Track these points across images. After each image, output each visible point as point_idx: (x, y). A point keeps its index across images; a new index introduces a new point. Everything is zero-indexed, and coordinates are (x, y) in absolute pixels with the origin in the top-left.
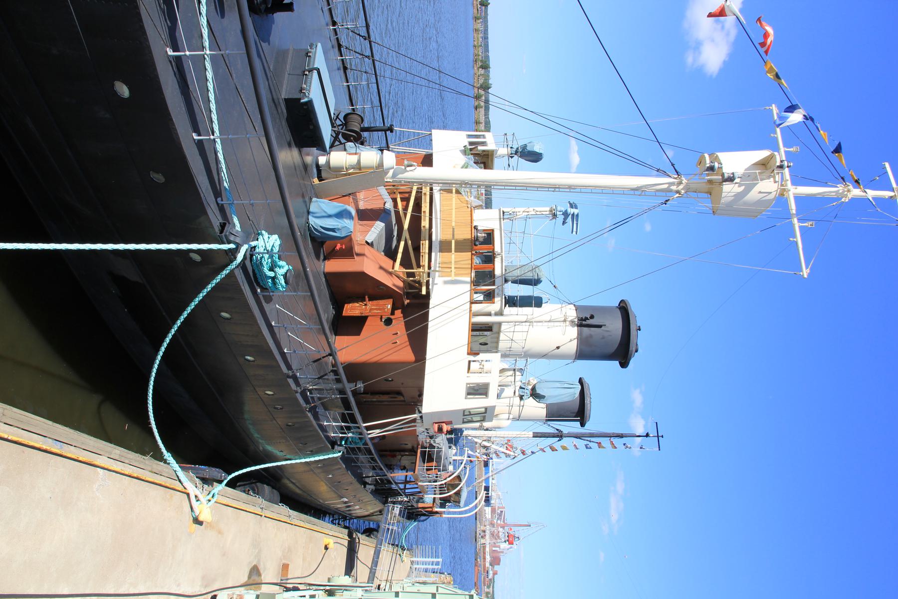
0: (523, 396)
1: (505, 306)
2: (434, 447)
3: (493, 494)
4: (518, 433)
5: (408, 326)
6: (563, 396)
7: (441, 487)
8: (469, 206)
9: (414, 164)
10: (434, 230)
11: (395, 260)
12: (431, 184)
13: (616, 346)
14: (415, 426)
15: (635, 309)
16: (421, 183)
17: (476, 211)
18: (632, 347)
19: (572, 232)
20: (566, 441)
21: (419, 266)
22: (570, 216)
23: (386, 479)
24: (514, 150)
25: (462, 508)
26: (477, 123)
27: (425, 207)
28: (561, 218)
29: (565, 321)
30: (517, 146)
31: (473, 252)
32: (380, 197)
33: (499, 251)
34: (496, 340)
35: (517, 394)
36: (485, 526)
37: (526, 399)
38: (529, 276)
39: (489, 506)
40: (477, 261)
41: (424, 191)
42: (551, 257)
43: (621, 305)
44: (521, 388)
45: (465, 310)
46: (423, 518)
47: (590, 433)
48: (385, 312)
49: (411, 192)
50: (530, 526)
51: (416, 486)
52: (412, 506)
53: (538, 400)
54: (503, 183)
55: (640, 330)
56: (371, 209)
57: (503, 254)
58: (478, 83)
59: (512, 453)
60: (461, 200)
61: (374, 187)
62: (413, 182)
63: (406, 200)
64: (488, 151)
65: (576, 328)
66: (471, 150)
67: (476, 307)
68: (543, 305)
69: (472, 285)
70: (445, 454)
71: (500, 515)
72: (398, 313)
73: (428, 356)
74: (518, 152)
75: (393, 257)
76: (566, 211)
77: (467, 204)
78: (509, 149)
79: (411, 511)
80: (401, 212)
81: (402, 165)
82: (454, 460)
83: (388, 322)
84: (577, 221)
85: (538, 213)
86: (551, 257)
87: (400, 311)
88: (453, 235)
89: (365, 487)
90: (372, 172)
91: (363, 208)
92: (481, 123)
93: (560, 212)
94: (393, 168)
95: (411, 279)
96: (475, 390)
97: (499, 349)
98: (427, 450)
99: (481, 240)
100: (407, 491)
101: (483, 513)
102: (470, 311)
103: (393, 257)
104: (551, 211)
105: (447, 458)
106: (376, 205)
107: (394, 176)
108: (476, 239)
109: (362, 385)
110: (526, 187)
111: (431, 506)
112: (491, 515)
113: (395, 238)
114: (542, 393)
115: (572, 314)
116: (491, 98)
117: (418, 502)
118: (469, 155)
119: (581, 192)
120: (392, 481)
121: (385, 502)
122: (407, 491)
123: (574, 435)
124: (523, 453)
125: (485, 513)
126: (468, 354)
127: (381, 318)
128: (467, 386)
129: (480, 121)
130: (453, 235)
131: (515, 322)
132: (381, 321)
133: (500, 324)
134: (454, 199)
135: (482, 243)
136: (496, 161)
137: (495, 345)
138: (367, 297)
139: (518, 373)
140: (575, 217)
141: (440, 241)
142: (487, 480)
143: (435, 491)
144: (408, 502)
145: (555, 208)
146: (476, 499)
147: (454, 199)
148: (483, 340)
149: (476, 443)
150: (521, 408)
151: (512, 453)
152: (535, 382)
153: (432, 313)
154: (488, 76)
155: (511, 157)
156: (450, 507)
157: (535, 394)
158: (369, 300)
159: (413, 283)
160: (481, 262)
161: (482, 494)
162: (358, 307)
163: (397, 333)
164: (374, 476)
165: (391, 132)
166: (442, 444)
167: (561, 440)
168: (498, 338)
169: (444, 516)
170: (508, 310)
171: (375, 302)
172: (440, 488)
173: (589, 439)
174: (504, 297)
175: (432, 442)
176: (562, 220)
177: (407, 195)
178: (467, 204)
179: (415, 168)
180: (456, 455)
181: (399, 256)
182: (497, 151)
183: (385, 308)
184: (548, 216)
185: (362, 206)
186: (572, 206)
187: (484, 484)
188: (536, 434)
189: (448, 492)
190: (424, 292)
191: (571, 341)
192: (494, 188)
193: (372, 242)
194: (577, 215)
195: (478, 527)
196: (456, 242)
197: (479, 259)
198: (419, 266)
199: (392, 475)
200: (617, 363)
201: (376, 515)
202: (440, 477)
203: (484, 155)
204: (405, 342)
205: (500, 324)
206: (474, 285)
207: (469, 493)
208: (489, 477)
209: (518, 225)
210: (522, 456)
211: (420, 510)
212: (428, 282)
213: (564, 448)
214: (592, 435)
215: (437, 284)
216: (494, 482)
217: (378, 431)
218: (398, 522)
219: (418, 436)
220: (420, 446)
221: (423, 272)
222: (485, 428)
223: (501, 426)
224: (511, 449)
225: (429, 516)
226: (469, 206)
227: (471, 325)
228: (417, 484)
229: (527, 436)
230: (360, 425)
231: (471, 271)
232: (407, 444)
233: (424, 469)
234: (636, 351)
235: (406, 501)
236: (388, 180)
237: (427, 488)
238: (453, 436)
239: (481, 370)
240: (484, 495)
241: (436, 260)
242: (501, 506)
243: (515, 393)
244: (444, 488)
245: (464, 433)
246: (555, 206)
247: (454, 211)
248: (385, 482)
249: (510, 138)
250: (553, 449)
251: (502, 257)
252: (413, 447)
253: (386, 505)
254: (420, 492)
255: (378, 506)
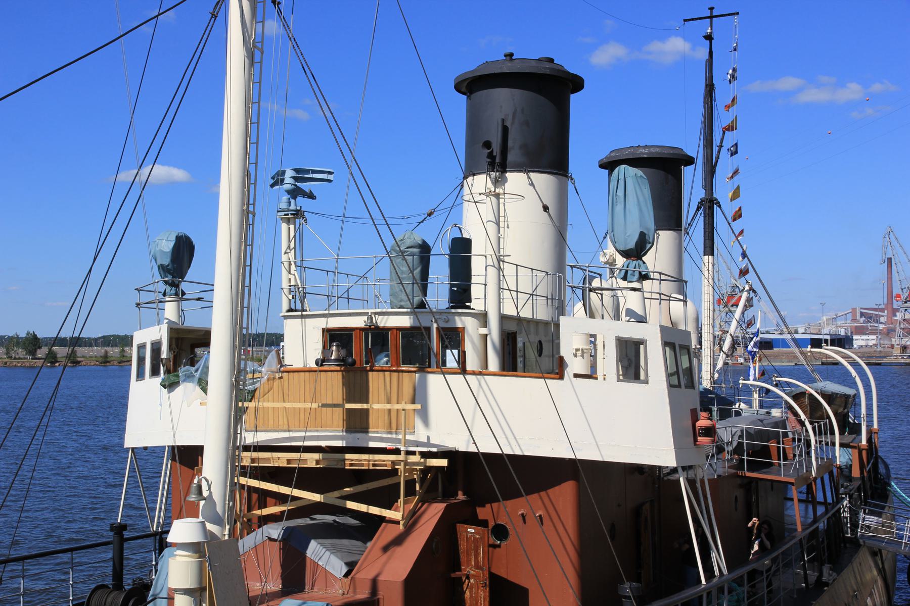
0: (640, 273)
1: (469, 308)
2: (740, 445)
3: (826, 331)
4: (705, 282)
5: (511, 494)
6: (641, 199)
7: (818, 432)
8: (277, 375)
9: (196, 481)
10: (323, 444)
11: (382, 519)
12: (235, 449)
13: (541, 98)
14: (702, 481)
15: (470, 65)
16: (235, 468)
17: (287, 362)
18: (545, 68)
19: (330, 181)
20: (722, 191)
21: (394, 472)
22: (299, 184)
23: (809, 541)
24: (168, 288)
25: (858, 391)
26: (105, 360)
27: (280, 460)
28: (302, 202)
29: (497, 196)
30: (161, 283)
31: (368, 368)
32: (260, 550)
33: (365, 318)
34: (532, 328)
35: (636, 285)
36: (892, 346)
37: (647, 268)
38: (413, 260)
39: (852, 340)
40: (382, 361)
41: (246, 462)
42: (380, 222)
43: (464, 90)
44: (625, 278)
45: (480, 384)
46: (882, 469)
47: (705, 146)
48: (482, 538)
49: (249, 487)
50: (890, 259)
51: (819, 481)
52: (859, 489)
53: (648, 246)
54: (237, 310)
55: (511, 55)
56: (282, 566)
57: (370, 311)
58: (25, 358)
59: (745, 295)
60: (266, 390)
61: (240, 561)
62: (233, 484)
63: (264, 497)
64: (171, 340)
65: (508, 175)
66: (168, 372)
67: (472, 363)
68: (466, 236)
69: (429, 370)
70: (752, 423)
71: (869, 317)
72: (483, 513)
73: (567, 455)
74: (173, 281)
75: (371, 525)
76: (288, 192)
77: (274, 379)
78: (167, 299)
79: (869, 494)
80: (290, 508)
81: (198, 505)
82: (761, 406)
83: (501, 532)
84: (307, 171)
85: (292, 245)
86: (380, 222)
87: (479, 510)
88: (335, 406)
89: (827, 584)
90: (210, 564)
91: (279, 581)
92: (106, 352)
93: (290, 203)
94: (203, 523)
95: (418, 488)
96: (630, 365)
97: (550, 319)
98: (745, 458)
99: (343, 353)
100: (829, 500)
101: (867, 350)
102: (480, 373)
103: (371, 525)
104: (288, 221)
105: (761, 421)
106: (274, 558)
107: (218, 521)
108: (341, 361)
109: (627, 585)
110: (245, 266)
111: (856, 451)
112: (869, 334)
113: (337, 519)
114: (635, 238)
115: (481, 182)
116: (66, 333)
117: (850, 479)
118: (178, 376)
119: (256, 164)
120: (812, 529)
121: (855, 544)
122: (829, 500)
123: (709, 179)
124: (743, 273)
125: (866, 346)
126: (561, 378)
127: (495, 546)
128: (622, 381)
129: (102, 354)
130: (335, 406)
131: (500, 288)
132: (499, 546)
133: (503, 318)
134: (266, 405)
135: (350, 354)
136: (192, 322)
137: (541, 328)
138: (453, 575)
139: (596, 283)
140: (301, 175)
141: (346, 432)
142: (799, 343)
143: (827, 444)
144: (851, 497)
145: (283, 213)
146: (837, 363)
147: (266, 405)
148: (532, 354)
149: (726, 364)
150: (663, 277)
151: (745, 295)
152: (610, 250)
153: (488, 446)
154: (11, 339)
155: (182, 295)
156: (857, 415)
157: (637, 252)
158: (460, 570)
159: (426, 484)
160: (385, 353)
161: (829, 351)
162: (471, 592)
163: (522, 514)
164: (804, 564)
165: (126, 529)
166: (734, 430)
167: (719, 202)
168: (528, 321)
169: (875, 426)
170: (476, 304)
171: (463, 558)
172: (820, 434)
173: (715, 149)
174: (453, 311)
175: (730, 449)
176: (306, 200)
177: (255, 496)
178: (274, 379)
179: (203, 480)
180: (749, 403)
181: (375, 510)
182: (170, 322)
183: (475, 538)
184: (297, 226)
185: (274, 585)
186: (278, 179)
187: (809, 348)
188: (708, 249)
189: (829, 417)
190: (444, 462)
191: (532, 184)
192: (247, 328)
193: (346, 564)
194: (297, 171)
195: (896, 361)
196: (349, 401)
197: (379, 357)
198: (394, 472)
199: (799, 529)
200: (574, 98)
201: (883, 563)
202: (799, 434)
203: (177, 346)
204: (541, 498)
205: (503, 318)
206: (430, 367)
207: (826, 378)
208: (795, 340)
209: (317, 283)
210: (751, 276)
211: (865, 474)
212: (425, 455)
213: (736, 194)
214: (708, 143)
215: (428, 438)
216: (801, 330)
217: (714, 555)
218: (893, 518)
219: (719, 476)
220: (740, 473)
221: (406, 463)
222: (698, 346)
223: (695, 316)
224: (737, 297)
225: (877, 457)
226: (277, 375)
227: (505, 373)
228: (815, 479)
229: (710, 265)
230: (704, 589)
231: (403, 371)
232: (736, 497)
233: (784, 465)
234: (551, 60)
235: (850, 502)
236: (227, 532)
237: (822, 459)
238: (715, 408)
239: (585, 355)
240: (829, 347)
241: (381, 440)
242: (850, 316)
243: (634, 289)
244: (820, 427)
245: (708, 387)
246: (279, 214)
247: (287, 405)
248: (814, 542)
249: (145, 297)
250: (738, 215)
251: (376, 313)
252: (741, 486)
253: (861, 541)
254: (831, 474)
255: (864, 559)
